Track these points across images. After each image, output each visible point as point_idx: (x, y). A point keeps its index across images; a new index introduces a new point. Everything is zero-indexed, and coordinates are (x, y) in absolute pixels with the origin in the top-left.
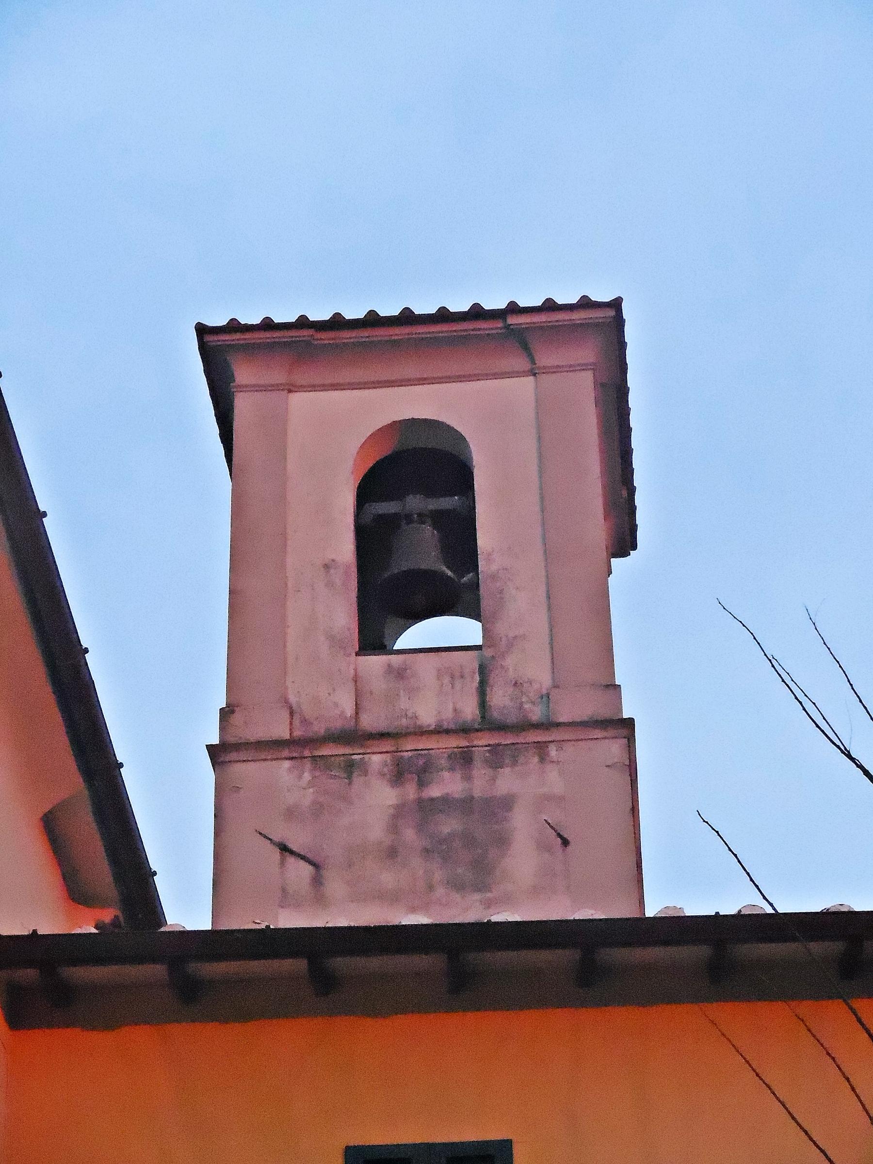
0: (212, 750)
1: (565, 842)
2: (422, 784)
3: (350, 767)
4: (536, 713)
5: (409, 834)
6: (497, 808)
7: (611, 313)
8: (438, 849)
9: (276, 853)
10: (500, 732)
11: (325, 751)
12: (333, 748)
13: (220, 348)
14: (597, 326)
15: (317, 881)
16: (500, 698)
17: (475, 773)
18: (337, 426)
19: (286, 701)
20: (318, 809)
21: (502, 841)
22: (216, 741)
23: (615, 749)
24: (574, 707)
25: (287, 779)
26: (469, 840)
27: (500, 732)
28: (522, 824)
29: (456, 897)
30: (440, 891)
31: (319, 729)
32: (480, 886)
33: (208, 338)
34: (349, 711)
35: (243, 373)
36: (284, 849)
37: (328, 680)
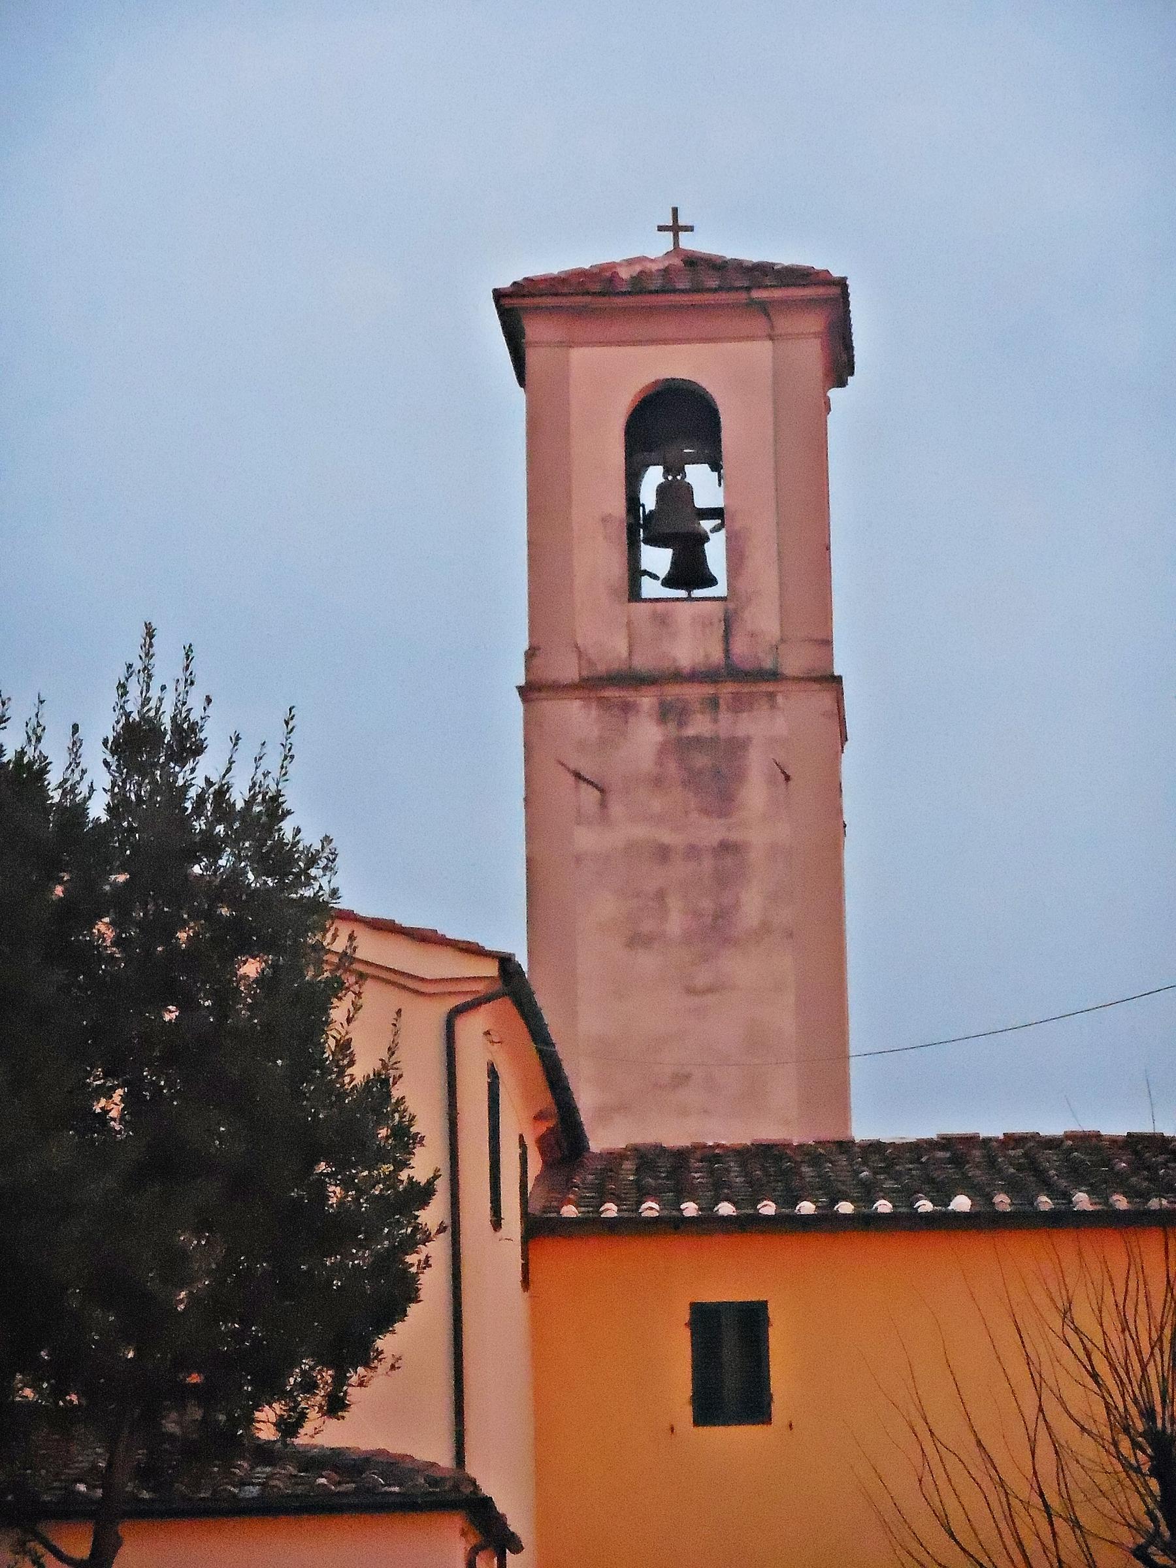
0: (520, 689)
1: (788, 778)
2: (681, 724)
3: (627, 708)
4: (768, 664)
5: (672, 767)
6: (737, 747)
7: (836, 291)
8: (692, 780)
9: (571, 779)
10: (742, 678)
11: (607, 693)
12: (610, 686)
13: (515, 306)
14: (826, 301)
15: (603, 804)
16: (740, 647)
17: (720, 717)
18: (612, 375)
19: (577, 646)
20: (604, 743)
21: (740, 776)
22: (522, 682)
23: (825, 700)
24: (794, 662)
25: (576, 717)
26: (717, 773)
27: (742, 678)
28: (757, 764)
29: (705, 821)
30: (694, 815)
31: (601, 668)
32: (723, 813)
33: (506, 302)
34: (623, 651)
35: (535, 330)
36: (578, 776)
37: (606, 638)
